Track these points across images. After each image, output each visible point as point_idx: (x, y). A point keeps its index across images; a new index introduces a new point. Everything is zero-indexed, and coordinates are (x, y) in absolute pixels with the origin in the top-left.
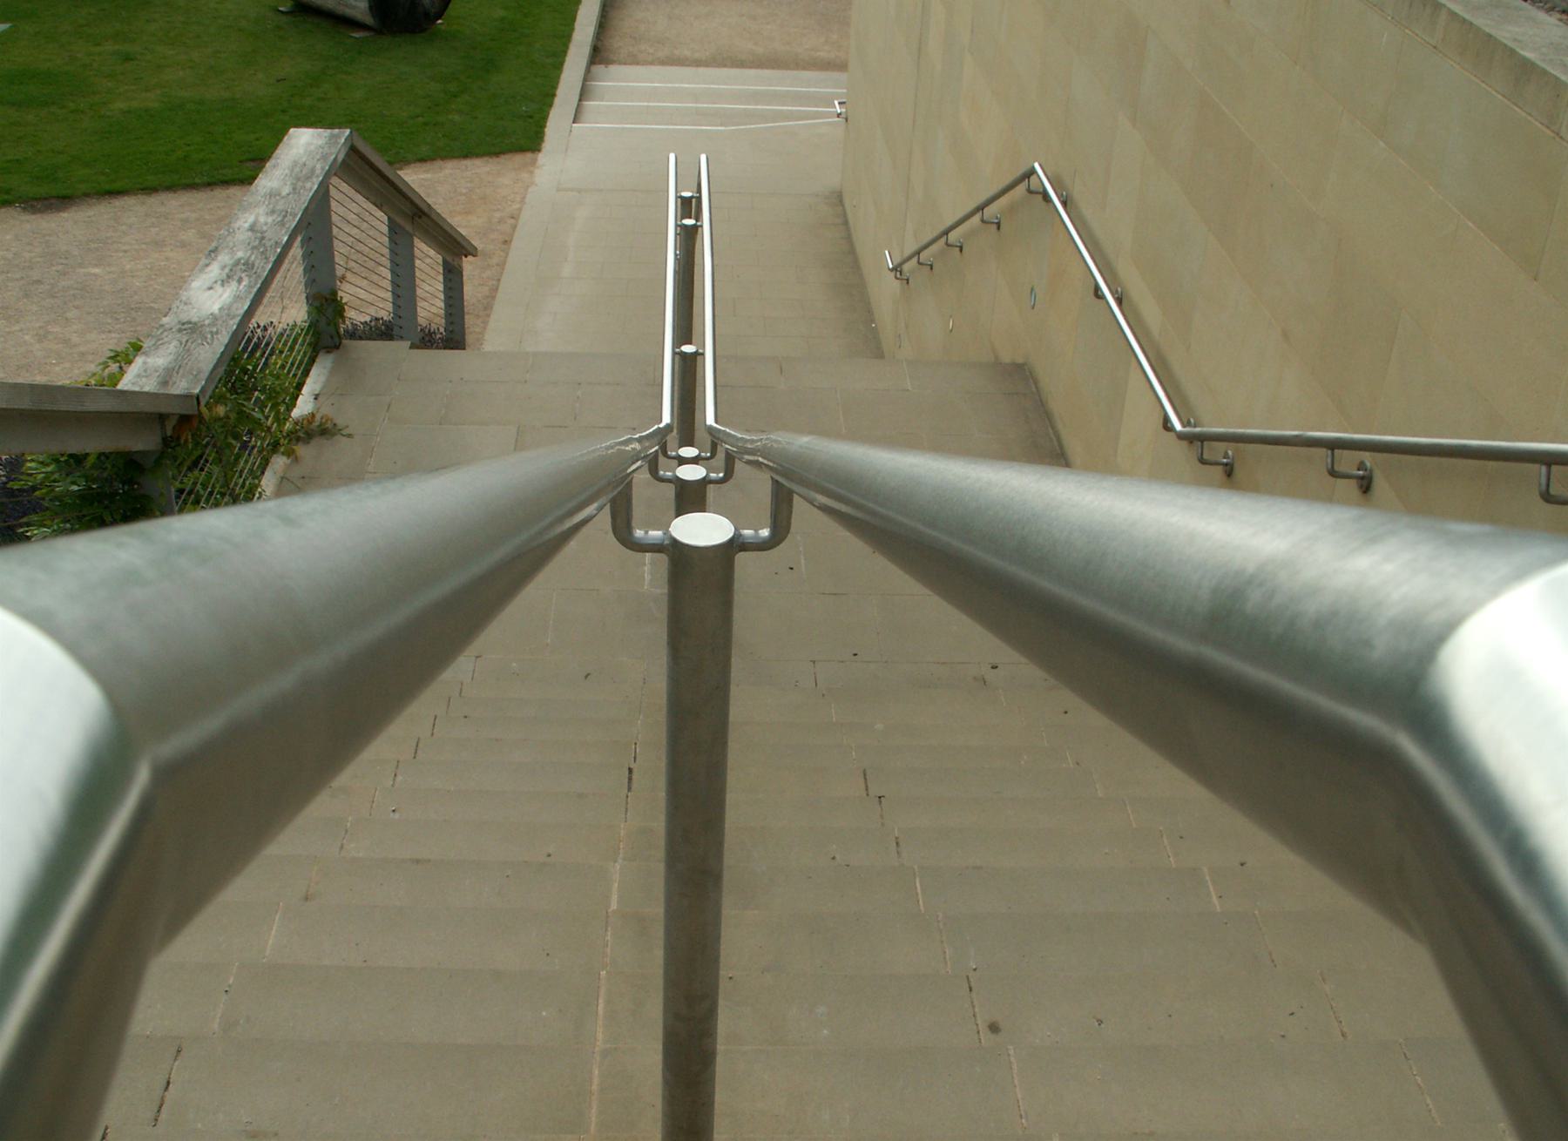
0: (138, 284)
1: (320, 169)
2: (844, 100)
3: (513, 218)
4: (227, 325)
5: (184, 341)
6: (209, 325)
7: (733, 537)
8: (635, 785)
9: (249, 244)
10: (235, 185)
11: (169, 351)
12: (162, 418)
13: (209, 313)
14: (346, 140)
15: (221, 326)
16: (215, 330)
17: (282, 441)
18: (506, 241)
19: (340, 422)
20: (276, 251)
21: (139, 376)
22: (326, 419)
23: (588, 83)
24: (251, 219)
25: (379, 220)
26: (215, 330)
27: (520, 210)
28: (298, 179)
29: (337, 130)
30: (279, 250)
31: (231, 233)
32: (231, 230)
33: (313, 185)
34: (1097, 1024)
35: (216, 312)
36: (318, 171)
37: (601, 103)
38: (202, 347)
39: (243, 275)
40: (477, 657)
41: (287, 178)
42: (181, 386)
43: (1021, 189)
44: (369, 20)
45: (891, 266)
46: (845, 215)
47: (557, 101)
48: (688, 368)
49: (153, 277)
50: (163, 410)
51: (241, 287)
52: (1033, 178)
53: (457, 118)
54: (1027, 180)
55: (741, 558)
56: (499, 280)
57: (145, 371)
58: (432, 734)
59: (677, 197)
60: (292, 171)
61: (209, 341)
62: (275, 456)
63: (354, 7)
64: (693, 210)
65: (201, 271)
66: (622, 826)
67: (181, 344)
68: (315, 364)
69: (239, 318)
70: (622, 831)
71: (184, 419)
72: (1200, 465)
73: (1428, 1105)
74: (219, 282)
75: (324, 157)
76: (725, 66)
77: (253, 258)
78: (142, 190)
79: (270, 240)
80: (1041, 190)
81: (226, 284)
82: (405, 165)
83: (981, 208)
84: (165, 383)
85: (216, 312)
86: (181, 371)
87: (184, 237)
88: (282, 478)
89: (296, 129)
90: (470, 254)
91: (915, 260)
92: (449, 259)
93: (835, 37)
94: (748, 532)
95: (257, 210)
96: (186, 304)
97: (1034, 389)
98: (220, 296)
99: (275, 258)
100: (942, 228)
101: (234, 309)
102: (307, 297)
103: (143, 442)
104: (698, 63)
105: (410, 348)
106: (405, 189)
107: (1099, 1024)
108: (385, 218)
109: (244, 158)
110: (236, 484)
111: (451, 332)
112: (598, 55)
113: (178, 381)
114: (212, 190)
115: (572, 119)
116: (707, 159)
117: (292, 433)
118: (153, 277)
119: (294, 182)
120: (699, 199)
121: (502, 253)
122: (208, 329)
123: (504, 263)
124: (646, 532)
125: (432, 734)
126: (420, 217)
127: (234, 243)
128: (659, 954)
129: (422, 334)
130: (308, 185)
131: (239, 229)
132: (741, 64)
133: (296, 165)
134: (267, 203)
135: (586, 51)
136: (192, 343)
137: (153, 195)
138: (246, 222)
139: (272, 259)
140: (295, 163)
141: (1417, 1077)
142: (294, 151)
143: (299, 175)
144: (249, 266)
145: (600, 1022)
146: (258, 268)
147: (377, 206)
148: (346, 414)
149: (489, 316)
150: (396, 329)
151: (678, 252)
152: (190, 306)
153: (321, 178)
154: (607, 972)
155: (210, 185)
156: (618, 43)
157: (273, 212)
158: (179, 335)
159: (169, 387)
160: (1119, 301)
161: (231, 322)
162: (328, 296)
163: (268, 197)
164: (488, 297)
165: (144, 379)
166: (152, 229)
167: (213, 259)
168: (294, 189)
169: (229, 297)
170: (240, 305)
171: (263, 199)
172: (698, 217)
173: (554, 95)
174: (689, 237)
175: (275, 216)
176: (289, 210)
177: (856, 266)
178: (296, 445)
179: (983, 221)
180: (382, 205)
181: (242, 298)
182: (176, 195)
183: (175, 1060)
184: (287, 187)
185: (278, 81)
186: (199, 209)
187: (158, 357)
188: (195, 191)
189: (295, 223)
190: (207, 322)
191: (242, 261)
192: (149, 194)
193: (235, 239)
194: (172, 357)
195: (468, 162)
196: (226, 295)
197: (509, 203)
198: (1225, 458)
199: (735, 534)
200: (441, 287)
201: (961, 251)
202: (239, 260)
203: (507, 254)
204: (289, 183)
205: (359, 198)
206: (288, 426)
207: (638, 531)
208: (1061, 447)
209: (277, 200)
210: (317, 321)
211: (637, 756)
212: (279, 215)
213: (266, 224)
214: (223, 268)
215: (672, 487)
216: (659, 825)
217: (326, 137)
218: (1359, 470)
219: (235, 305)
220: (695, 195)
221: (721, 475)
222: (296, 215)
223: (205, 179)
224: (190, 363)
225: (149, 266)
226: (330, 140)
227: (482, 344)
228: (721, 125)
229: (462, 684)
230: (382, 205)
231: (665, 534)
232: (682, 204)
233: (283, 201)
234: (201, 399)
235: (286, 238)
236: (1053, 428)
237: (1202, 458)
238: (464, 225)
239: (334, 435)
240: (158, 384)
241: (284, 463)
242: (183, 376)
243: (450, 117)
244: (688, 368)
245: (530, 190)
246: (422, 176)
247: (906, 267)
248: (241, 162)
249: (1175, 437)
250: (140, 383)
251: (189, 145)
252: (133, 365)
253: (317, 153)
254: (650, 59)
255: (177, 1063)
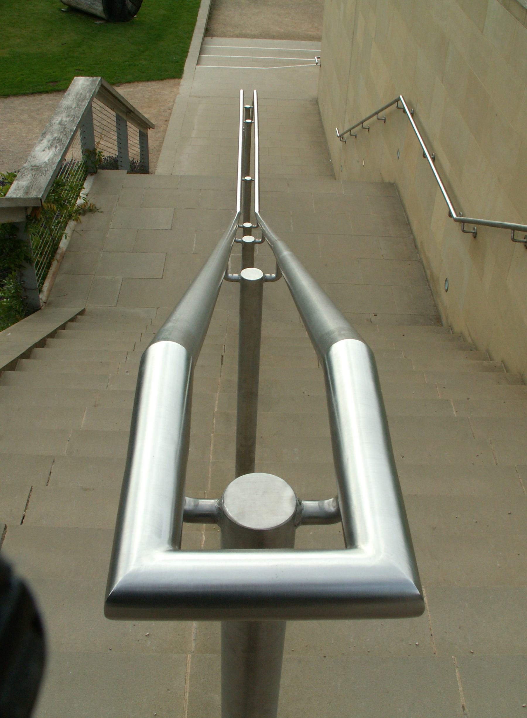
0: (3, 140)
1: (88, 96)
2: (320, 57)
3: (170, 109)
4: (52, 167)
5: (34, 174)
6: (44, 167)
7: (263, 277)
8: (224, 363)
9: (59, 131)
10: (44, 94)
11: (28, 179)
12: (26, 208)
13: (44, 162)
14: (99, 82)
15: (49, 167)
16: (46, 169)
17: (73, 215)
18: (167, 120)
19: (98, 206)
20: (71, 134)
21: (15, 190)
22: (92, 205)
23: (203, 46)
24: (60, 119)
25: (112, 114)
26: (46, 169)
27: (173, 105)
28: (79, 101)
29: (95, 78)
30: (72, 133)
31: (51, 125)
32: (51, 124)
33: (86, 104)
34: (401, 457)
35: (47, 161)
36: (88, 97)
37: (209, 56)
38: (41, 177)
39: (57, 145)
40: (158, 308)
41: (74, 100)
42: (34, 194)
43: (394, 106)
44: (103, 15)
45: (338, 135)
46: (319, 110)
47: (189, 54)
48: (248, 186)
49: (9, 136)
50: (28, 205)
51: (57, 150)
52: (399, 102)
53: (144, 62)
54: (397, 102)
55: (265, 284)
56: (164, 138)
57: (18, 187)
58: (140, 341)
59: (243, 108)
60: (76, 97)
61: (45, 175)
62: (70, 221)
63: (96, 10)
64: (251, 113)
65: (39, 143)
66: (219, 379)
67: (33, 175)
68: (86, 180)
69: (57, 164)
70: (219, 381)
71: (35, 209)
72: (463, 233)
73: (523, 490)
74: (47, 148)
75: (90, 90)
76: (266, 38)
77: (61, 137)
78: (3, 96)
79: (68, 129)
80: (403, 107)
81: (50, 149)
82: (121, 85)
83: (377, 113)
84: (27, 193)
85: (47, 161)
86: (33, 188)
87: (22, 118)
88: (74, 231)
89: (77, 77)
90: (152, 128)
91: (349, 133)
92: (142, 130)
93: (316, 24)
94: (268, 275)
95: (62, 115)
96: (33, 157)
97: (398, 195)
98: (48, 154)
99: (71, 137)
100: (361, 120)
101: (54, 160)
102: (82, 152)
103: (18, 218)
104: (254, 37)
105: (127, 173)
106: (123, 102)
107: (403, 458)
108: (114, 114)
109: (48, 81)
110: (55, 233)
111: (143, 162)
112: (208, 32)
113: (32, 192)
114: (34, 96)
115: (196, 64)
116: (257, 92)
117: (77, 211)
118: (9, 136)
119: (77, 102)
120: (253, 108)
121: (165, 126)
122: (44, 169)
123: (166, 130)
124: (233, 275)
125: (140, 341)
126: (130, 113)
127: (53, 130)
128: (234, 428)
129: (130, 164)
130: (84, 103)
131: (54, 124)
132: (273, 37)
133: (78, 94)
134: (66, 111)
135: (203, 30)
136: (37, 175)
137: (8, 98)
138: (57, 120)
139: (70, 137)
140: (78, 93)
141: (520, 479)
142: (77, 88)
143: (79, 99)
144: (60, 140)
145: (211, 453)
146: (64, 142)
147: (111, 109)
148: (100, 202)
149: (159, 155)
150: (119, 163)
151: (244, 128)
152: (36, 159)
153: (89, 100)
154: (214, 434)
155: (33, 94)
156: (217, 27)
157: (69, 116)
158: (31, 172)
159: (29, 195)
160: (433, 160)
161: (53, 166)
162: (92, 151)
163: (66, 109)
164: (158, 146)
165: (18, 191)
166: (8, 114)
167: (44, 138)
168: (78, 105)
169: (52, 154)
170: (57, 158)
171: (64, 110)
172: (252, 118)
173: (188, 52)
174: (248, 127)
175: (69, 118)
176: (76, 115)
177: (323, 133)
178: (79, 215)
179: (378, 119)
180: (114, 109)
181: (57, 155)
182: (18, 98)
183: (53, 464)
184: (75, 104)
185: (62, 44)
186: (29, 105)
187: (23, 181)
188: (26, 96)
189: (79, 121)
190: (43, 166)
191: (57, 138)
192: (6, 98)
193: (53, 129)
194: (29, 181)
195: (149, 83)
196: (50, 154)
197: (168, 102)
198: (473, 230)
199: (263, 276)
200: (138, 142)
201: (369, 131)
202: (55, 138)
203: (167, 126)
204: (75, 102)
205: (107, 108)
206: (75, 208)
207: (230, 274)
208: (408, 220)
209: (71, 110)
210: (87, 161)
211: (225, 351)
212: (71, 118)
213: (66, 121)
214: (49, 141)
215: (241, 244)
216: (235, 378)
217: (90, 81)
218: (525, 239)
219: (55, 158)
220: (251, 107)
221: (260, 240)
222: (79, 117)
223: (31, 91)
224: (37, 184)
225: (7, 131)
226: (92, 82)
227: (156, 168)
228: (264, 67)
229: (152, 319)
230: (114, 109)
231: (239, 275)
232: (246, 110)
233: (73, 111)
234: (42, 200)
235: (75, 128)
236: (405, 212)
237: (464, 230)
238: (147, 113)
239: (95, 211)
240: (24, 193)
241: (74, 224)
242: (34, 190)
243: (141, 62)
244: (248, 186)
245: (177, 96)
246: (128, 90)
247: (345, 136)
248: (47, 83)
249: (453, 220)
250: (17, 193)
251: (23, 75)
252: (13, 185)
253: (87, 89)
254: (231, 35)
255: (53, 465)
